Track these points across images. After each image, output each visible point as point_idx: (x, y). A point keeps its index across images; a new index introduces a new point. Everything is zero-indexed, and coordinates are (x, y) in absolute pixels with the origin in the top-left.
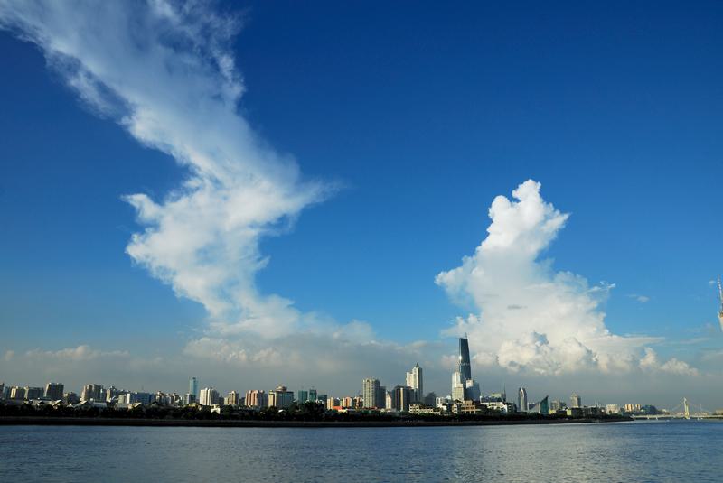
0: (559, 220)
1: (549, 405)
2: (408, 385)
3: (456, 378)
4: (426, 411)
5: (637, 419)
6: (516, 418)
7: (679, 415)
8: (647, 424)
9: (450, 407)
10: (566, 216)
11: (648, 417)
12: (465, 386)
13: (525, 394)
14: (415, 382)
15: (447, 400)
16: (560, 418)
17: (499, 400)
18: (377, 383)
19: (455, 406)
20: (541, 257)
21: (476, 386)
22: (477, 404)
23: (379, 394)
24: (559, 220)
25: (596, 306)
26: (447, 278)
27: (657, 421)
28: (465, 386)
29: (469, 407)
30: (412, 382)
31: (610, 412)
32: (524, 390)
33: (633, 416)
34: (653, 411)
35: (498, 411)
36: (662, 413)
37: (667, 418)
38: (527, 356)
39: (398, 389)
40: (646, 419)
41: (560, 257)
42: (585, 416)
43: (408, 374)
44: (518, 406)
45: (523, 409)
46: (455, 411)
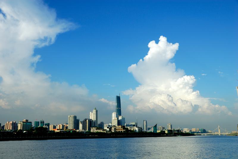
2: (90, 118)
7: (216, 133)
13: (146, 123)
18: (75, 117)
21: (123, 119)
23: (76, 123)
28: (118, 119)
34: (204, 131)
35: (133, 131)
39: (86, 120)
46: (113, 131)
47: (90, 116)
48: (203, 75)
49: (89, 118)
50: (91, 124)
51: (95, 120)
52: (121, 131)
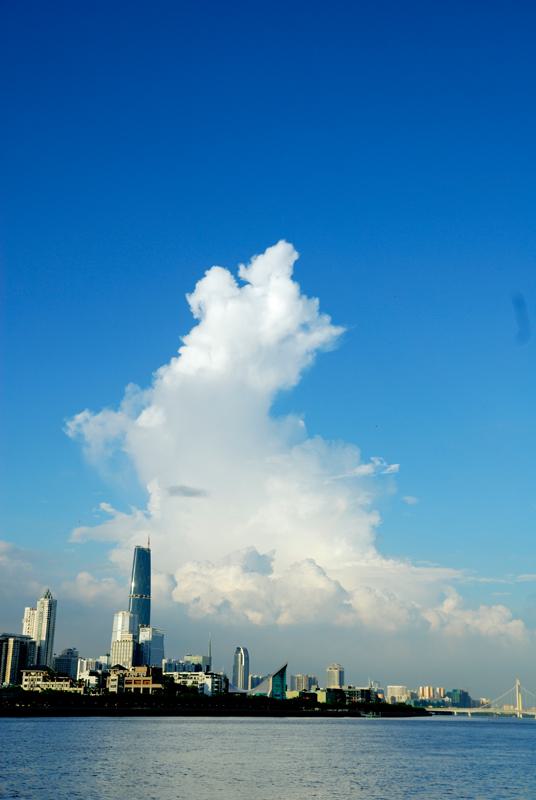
0: (326, 333)
1: (288, 681)
2: (25, 633)
3: (121, 623)
4: (55, 686)
5: (437, 713)
6: (226, 703)
7: (507, 709)
8: (467, 722)
9: (103, 679)
10: (338, 331)
11: (455, 710)
12: (136, 637)
13: (247, 659)
14: (40, 625)
15: (99, 666)
16: (304, 706)
17: (198, 668)
19: (114, 676)
20: (283, 404)
21: (158, 639)
22: (156, 674)
24: (326, 333)
25: (368, 502)
26: (90, 426)
27: (470, 718)
28: (136, 637)
29: (140, 679)
30: (33, 627)
31: (393, 698)
32: (245, 651)
33: (430, 708)
34: (464, 700)
35: (193, 689)
37: (486, 714)
38: (230, 582)
40: (450, 713)
41: (318, 404)
42: (346, 704)
43: (27, 609)
44: (230, 682)
45: (240, 689)
46: (112, 686)
47: (25, 625)
49: (17, 633)
51: (44, 638)
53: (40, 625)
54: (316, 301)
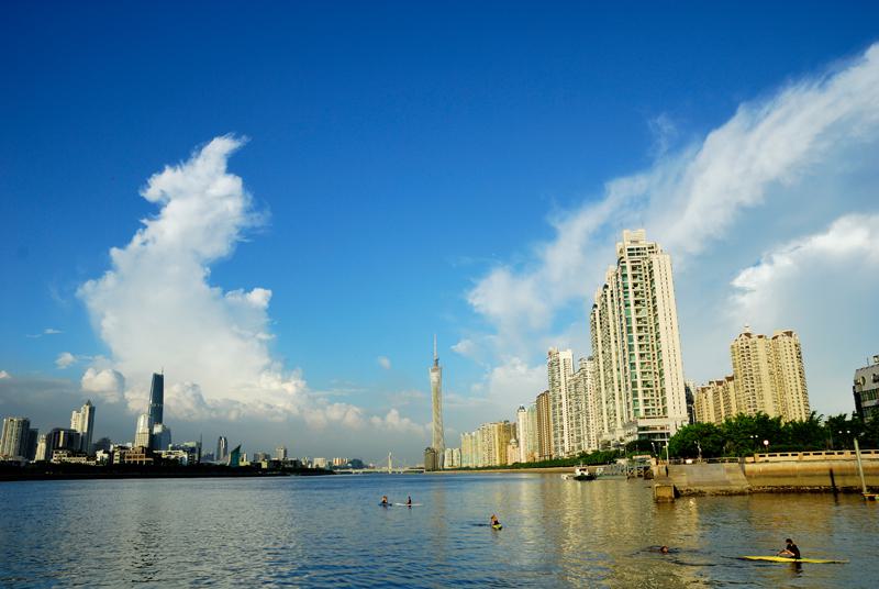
2: (72, 428)
3: (142, 424)
4: (74, 460)
6: (199, 468)
7: (384, 469)
13: (226, 444)
16: (253, 471)
18: (25, 424)
21: (166, 432)
23: (27, 439)
24: (260, 220)
28: (151, 431)
30: (78, 423)
34: (358, 464)
35: (175, 460)
36: (367, 467)
39: (57, 432)
42: (280, 469)
46: (116, 461)
47: (73, 424)
48: (50, 331)
49: (65, 427)
50: (73, 442)
51: (85, 431)
52: (141, 462)
53: (84, 422)
54: (167, 167)
